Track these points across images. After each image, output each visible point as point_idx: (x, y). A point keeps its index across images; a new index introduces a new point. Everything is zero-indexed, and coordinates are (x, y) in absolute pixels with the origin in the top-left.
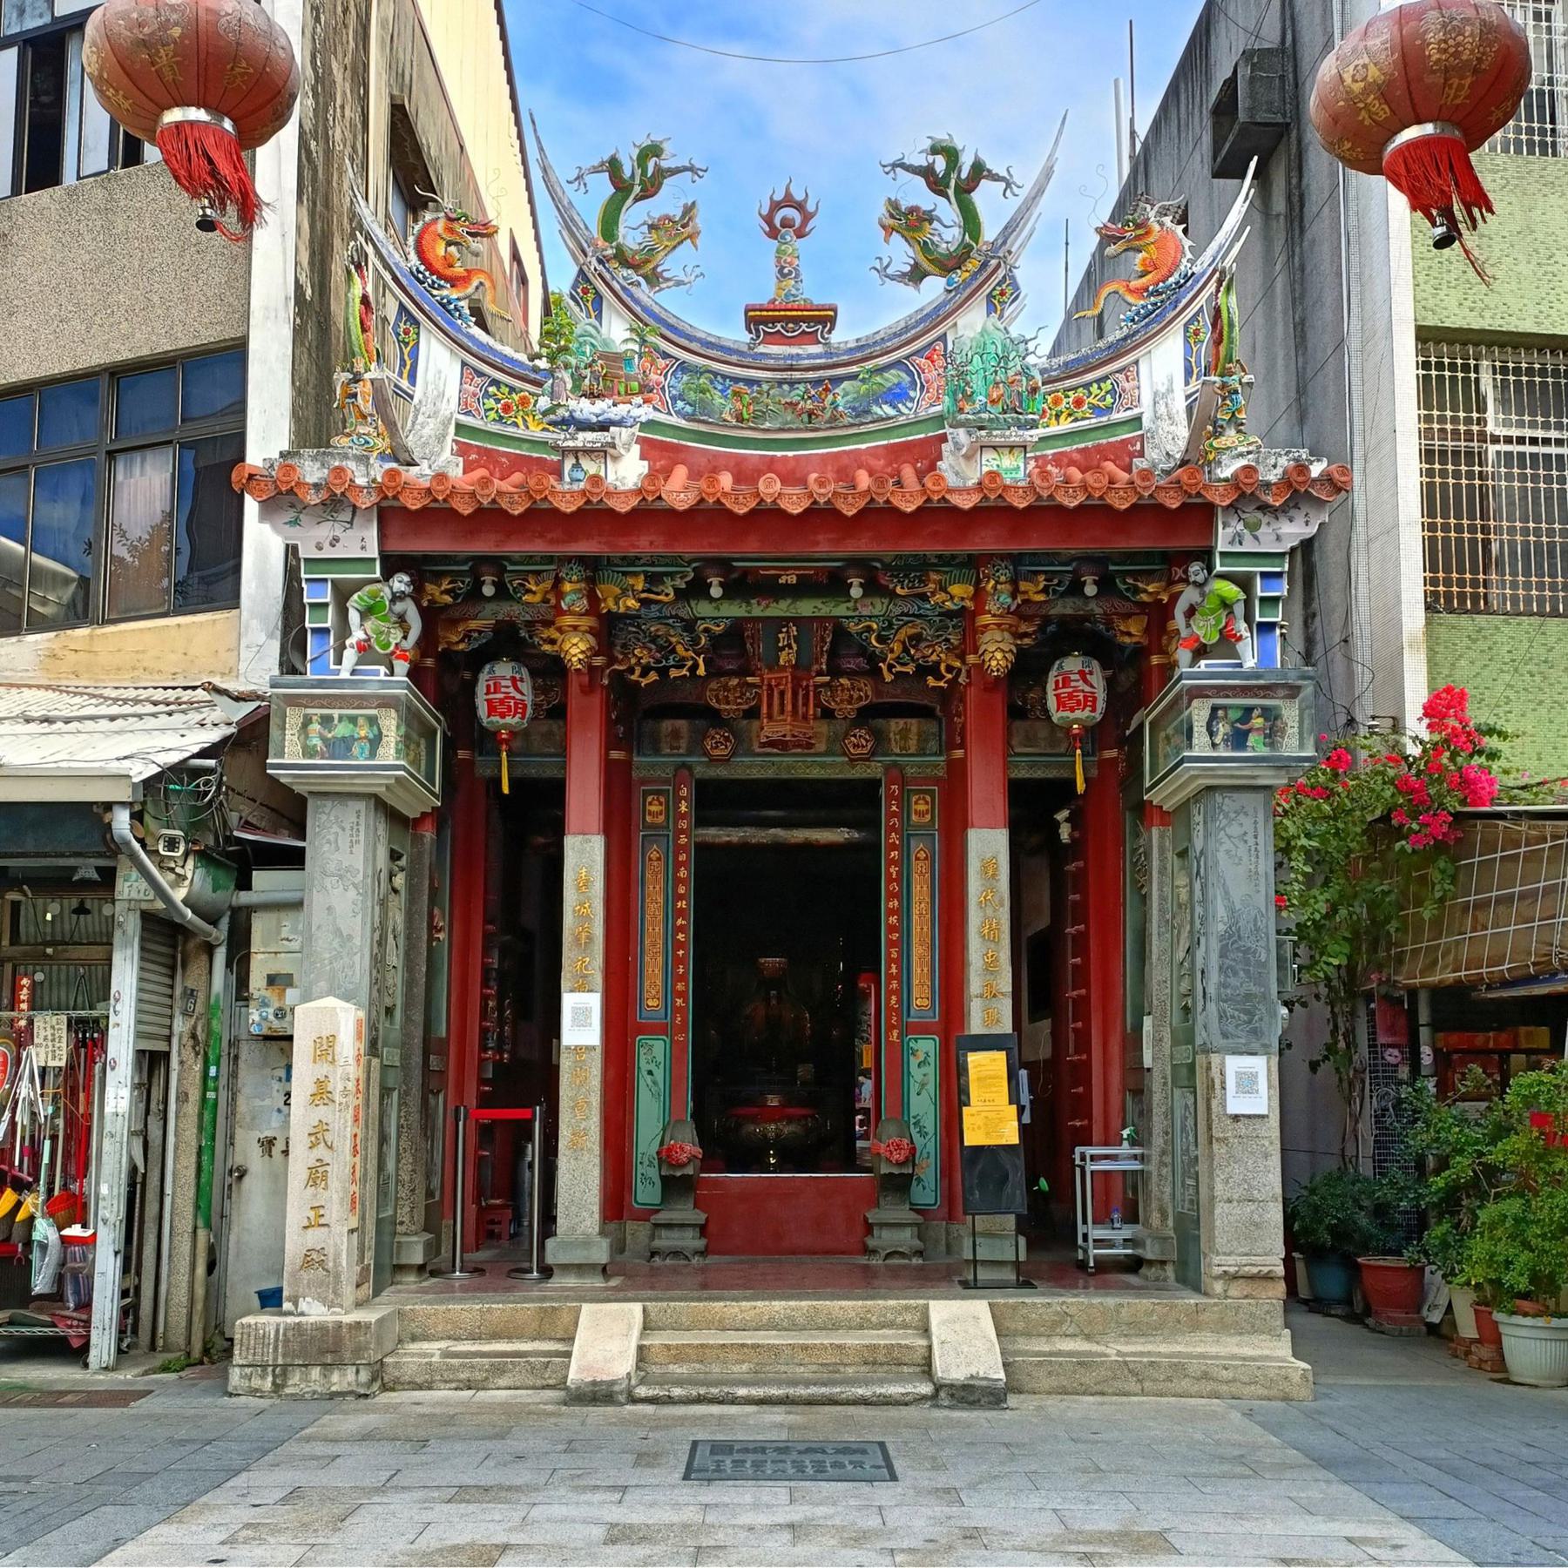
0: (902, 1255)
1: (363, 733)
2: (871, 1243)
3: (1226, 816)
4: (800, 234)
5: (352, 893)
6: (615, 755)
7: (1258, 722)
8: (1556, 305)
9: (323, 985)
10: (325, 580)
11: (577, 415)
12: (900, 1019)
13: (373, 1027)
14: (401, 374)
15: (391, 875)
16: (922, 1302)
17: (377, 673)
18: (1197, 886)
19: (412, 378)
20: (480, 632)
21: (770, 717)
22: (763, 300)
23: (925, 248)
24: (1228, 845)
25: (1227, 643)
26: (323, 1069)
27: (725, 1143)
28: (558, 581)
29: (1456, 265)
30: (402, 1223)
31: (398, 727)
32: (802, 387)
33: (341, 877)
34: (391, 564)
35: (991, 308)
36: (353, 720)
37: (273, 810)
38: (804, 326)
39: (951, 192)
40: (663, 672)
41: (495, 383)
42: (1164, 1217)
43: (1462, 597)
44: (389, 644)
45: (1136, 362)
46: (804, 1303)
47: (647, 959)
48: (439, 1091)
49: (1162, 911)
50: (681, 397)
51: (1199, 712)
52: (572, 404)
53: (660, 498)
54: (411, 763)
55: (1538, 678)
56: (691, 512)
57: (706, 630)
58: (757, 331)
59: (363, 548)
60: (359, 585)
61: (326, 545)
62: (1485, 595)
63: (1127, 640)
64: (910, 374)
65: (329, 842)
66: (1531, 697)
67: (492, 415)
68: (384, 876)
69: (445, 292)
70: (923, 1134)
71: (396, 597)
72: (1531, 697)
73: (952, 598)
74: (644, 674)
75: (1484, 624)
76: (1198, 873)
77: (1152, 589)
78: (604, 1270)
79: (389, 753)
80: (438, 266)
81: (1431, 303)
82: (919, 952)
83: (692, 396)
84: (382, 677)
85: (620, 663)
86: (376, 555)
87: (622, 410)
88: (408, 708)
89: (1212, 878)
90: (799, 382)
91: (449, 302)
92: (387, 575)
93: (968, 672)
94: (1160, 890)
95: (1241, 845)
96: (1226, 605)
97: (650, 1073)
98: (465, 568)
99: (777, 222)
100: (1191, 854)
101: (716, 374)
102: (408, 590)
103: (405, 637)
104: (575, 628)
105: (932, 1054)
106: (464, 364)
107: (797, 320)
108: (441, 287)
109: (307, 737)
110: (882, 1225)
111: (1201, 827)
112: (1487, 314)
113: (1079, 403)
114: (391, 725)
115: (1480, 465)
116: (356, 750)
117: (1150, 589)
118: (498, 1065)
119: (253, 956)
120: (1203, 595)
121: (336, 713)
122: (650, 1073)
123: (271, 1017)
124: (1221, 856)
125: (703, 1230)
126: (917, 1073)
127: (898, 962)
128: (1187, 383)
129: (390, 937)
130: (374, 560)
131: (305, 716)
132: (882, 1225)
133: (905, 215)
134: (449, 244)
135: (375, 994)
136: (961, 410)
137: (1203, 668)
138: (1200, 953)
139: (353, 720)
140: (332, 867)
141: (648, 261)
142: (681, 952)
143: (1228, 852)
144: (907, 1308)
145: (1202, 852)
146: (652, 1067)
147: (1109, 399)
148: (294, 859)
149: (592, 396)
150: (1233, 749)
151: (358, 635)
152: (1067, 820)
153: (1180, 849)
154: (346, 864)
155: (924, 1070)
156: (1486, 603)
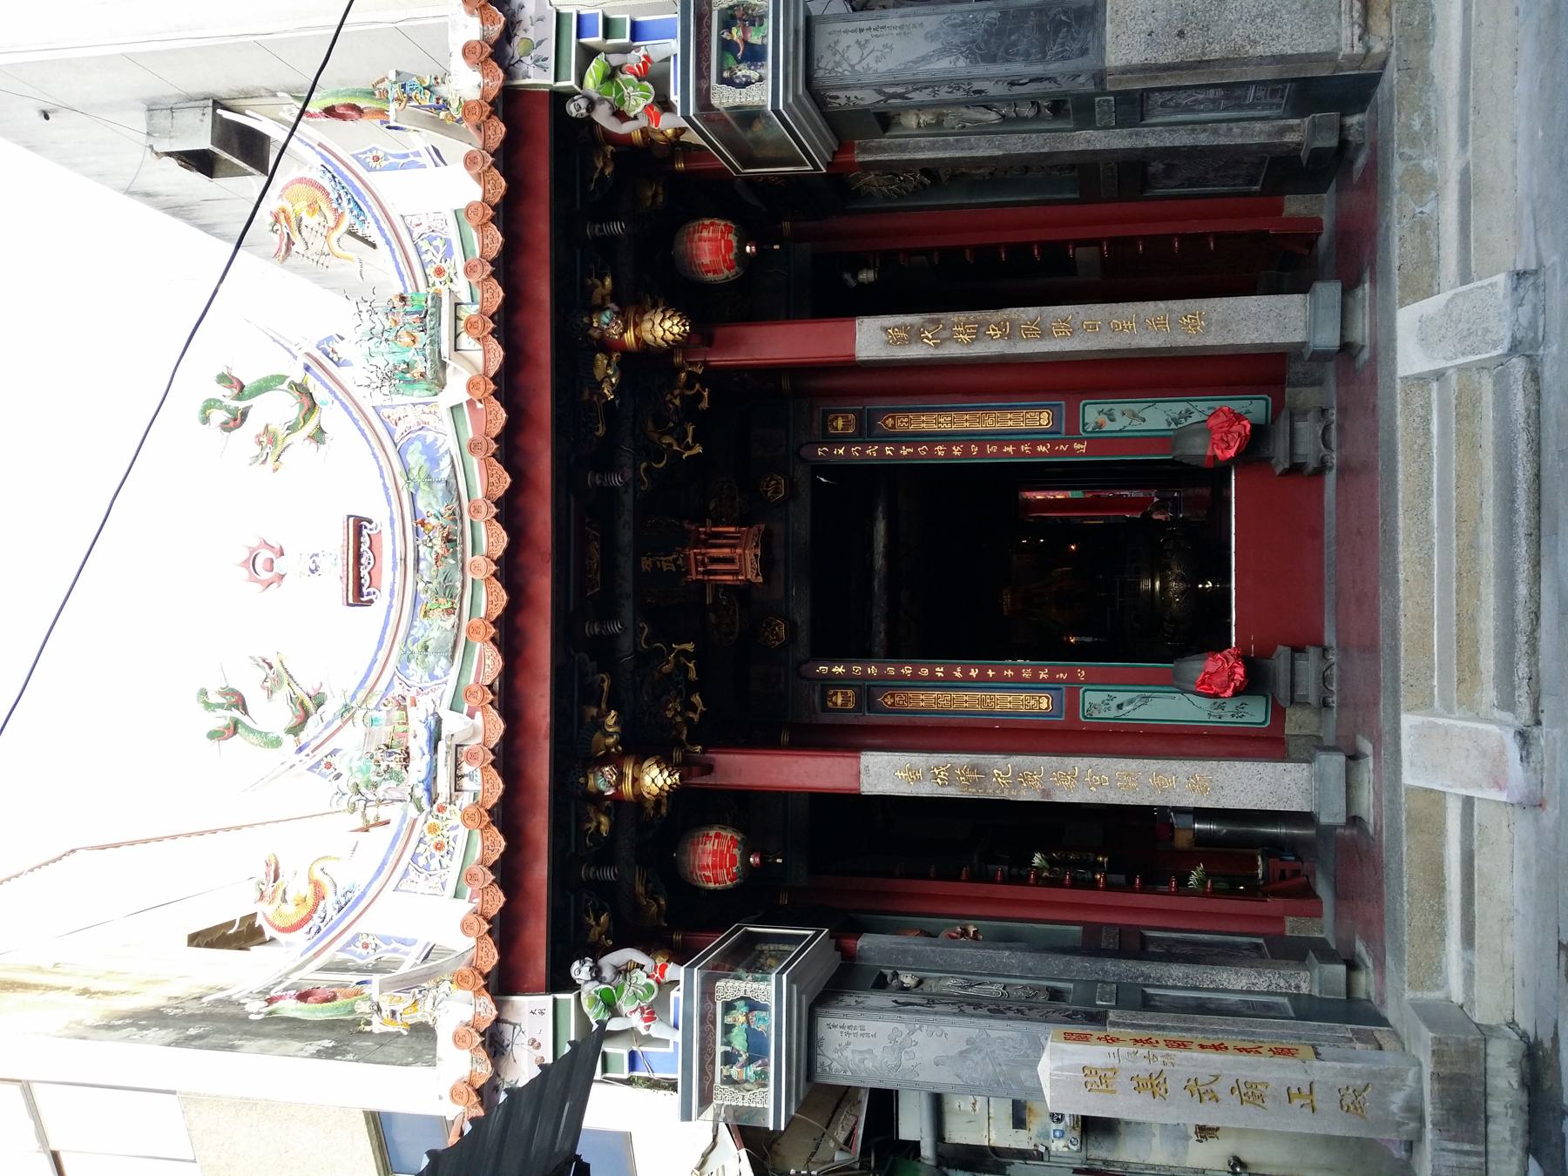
0: (1326, 429)
1: (742, 1019)
2: (1312, 464)
3: (838, 64)
5: (919, 1036)
6: (785, 738)
7: (736, 34)
9: (1024, 1074)
13: (1071, 1018)
14: (407, 954)
15: (903, 989)
16: (1399, 387)
17: (677, 999)
18: (917, 97)
19: (414, 942)
20: (648, 881)
21: (735, 573)
23: (292, 429)
24: (870, 61)
25: (654, 76)
26: (1123, 1080)
27: (1200, 629)
30: (1298, 987)
31: (739, 978)
32: (422, 549)
33: (901, 1049)
34: (559, 981)
36: (728, 1029)
37: (838, 1106)
40: (692, 688)
42: (1291, 129)
44: (647, 986)
46: (1401, 524)
47: (997, 708)
48: (1143, 937)
49: (947, 146)
51: (724, 98)
53: (490, 687)
54: (780, 960)
57: (647, 641)
59: (542, 1013)
63: (660, 198)
65: (863, 1061)
67: (445, 861)
68: (902, 998)
70: (1189, 414)
71: (597, 974)
73: (609, 377)
74: (694, 708)
76: (902, 96)
78: (1354, 757)
79: (766, 989)
80: (304, 912)
82: (991, 422)
83: (431, 659)
84: (681, 995)
85: (680, 733)
86: (549, 999)
88: (715, 968)
89: (908, 76)
92: (571, 986)
93: (691, 364)
94: (922, 149)
95: (870, 47)
96: (611, 75)
97: (1120, 706)
98: (572, 898)
100: (882, 107)
102: (589, 962)
103: (642, 967)
104: (635, 780)
105: (1100, 407)
107: (358, 556)
110: (1292, 453)
111: (852, 94)
113: (439, 272)
114: (729, 988)
116: (760, 1027)
117: (600, 164)
118: (1113, 868)
119: (993, 1143)
120: (602, 100)
121: (720, 1049)
122: (1120, 706)
123: (1061, 1126)
124: (882, 67)
125: (1297, 650)
128: (424, 166)
129: (971, 992)
130: (555, 1001)
131: (723, 1083)
132: (1292, 453)
134: (284, 900)
135: (1034, 1014)
138: (993, 90)
139: (728, 1029)
140: (891, 1060)
141: (302, 704)
142: (990, 673)
144: (1407, 403)
145: (880, 92)
146: (1113, 704)
147: (438, 242)
148: (884, 1103)
151: (636, 1021)
153: (877, 127)
154: (886, 1042)
155: (1117, 414)
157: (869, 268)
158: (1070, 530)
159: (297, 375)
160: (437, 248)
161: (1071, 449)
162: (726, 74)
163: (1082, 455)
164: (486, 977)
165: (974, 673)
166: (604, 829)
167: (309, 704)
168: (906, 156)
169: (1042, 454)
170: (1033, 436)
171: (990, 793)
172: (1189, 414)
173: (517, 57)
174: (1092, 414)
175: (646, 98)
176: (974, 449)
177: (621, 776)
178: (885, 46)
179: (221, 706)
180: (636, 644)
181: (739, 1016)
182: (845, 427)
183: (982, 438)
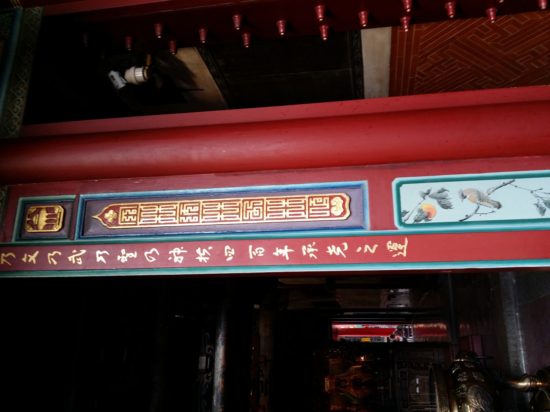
12: (370, 239)
105: (424, 187)
127: (322, 243)
152: (122, 75)
157: (138, 66)
158: (358, 347)
163: (401, 260)
169: (336, 260)
174: (413, 197)
176: (229, 252)
182: (49, 224)
183: (240, 238)
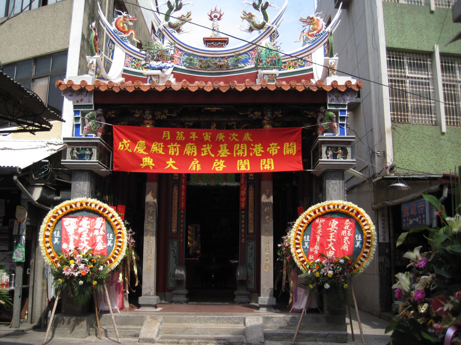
1: (88, 152)
4: (219, 19)
8: (423, 42)
10: (79, 111)
11: (152, 66)
14: (109, 57)
19: (112, 58)
22: (209, 36)
24: (332, 186)
28: (144, 111)
29: (396, 32)
32: (219, 59)
33: (81, 193)
35: (271, 39)
38: (219, 43)
39: (260, 9)
41: (135, 58)
43: (401, 119)
45: (311, 54)
50: (186, 62)
51: (324, 149)
52: (151, 63)
53: (171, 87)
55: (421, 142)
56: (179, 91)
57: (187, 124)
58: (207, 44)
60: (88, 112)
61: (80, 101)
62: (407, 119)
64: (249, 55)
66: (419, 146)
67: (133, 67)
69: (122, 35)
72: (419, 146)
73: (255, 116)
75: (407, 126)
77: (311, 114)
80: (121, 29)
81: (390, 41)
84: (94, 137)
86: (93, 104)
87: (164, 64)
90: (218, 57)
91: (123, 38)
95: (336, 186)
96: (331, 119)
97: (173, 250)
99: (213, 16)
101: (195, 55)
105: (254, 246)
106: (126, 54)
107: (217, 41)
108: (121, 34)
109: (73, 154)
112: (405, 44)
113: (295, 64)
115: (405, 84)
117: (311, 113)
121: (80, 147)
124: (330, 189)
126: (250, 251)
133: (248, 15)
136: (259, 65)
137: (325, 136)
142: (182, 216)
143: (332, 188)
146: (174, 249)
149: (157, 60)
150: (333, 159)
156: (408, 121)
159: (268, 24)
160: (302, 63)
161: (243, 238)
162: (329, 148)
163: (241, 241)
164: (98, 88)
165: (182, 212)
166: (136, 115)
167: (177, 28)
168: (314, 195)
170: (247, 228)
171: (146, 216)
172: (251, 269)
173: (335, 94)
175: (325, 127)
176: (243, 212)
177: (150, 120)
178: (335, 190)
179: (177, 4)
180: (187, 121)
181: (88, 152)
